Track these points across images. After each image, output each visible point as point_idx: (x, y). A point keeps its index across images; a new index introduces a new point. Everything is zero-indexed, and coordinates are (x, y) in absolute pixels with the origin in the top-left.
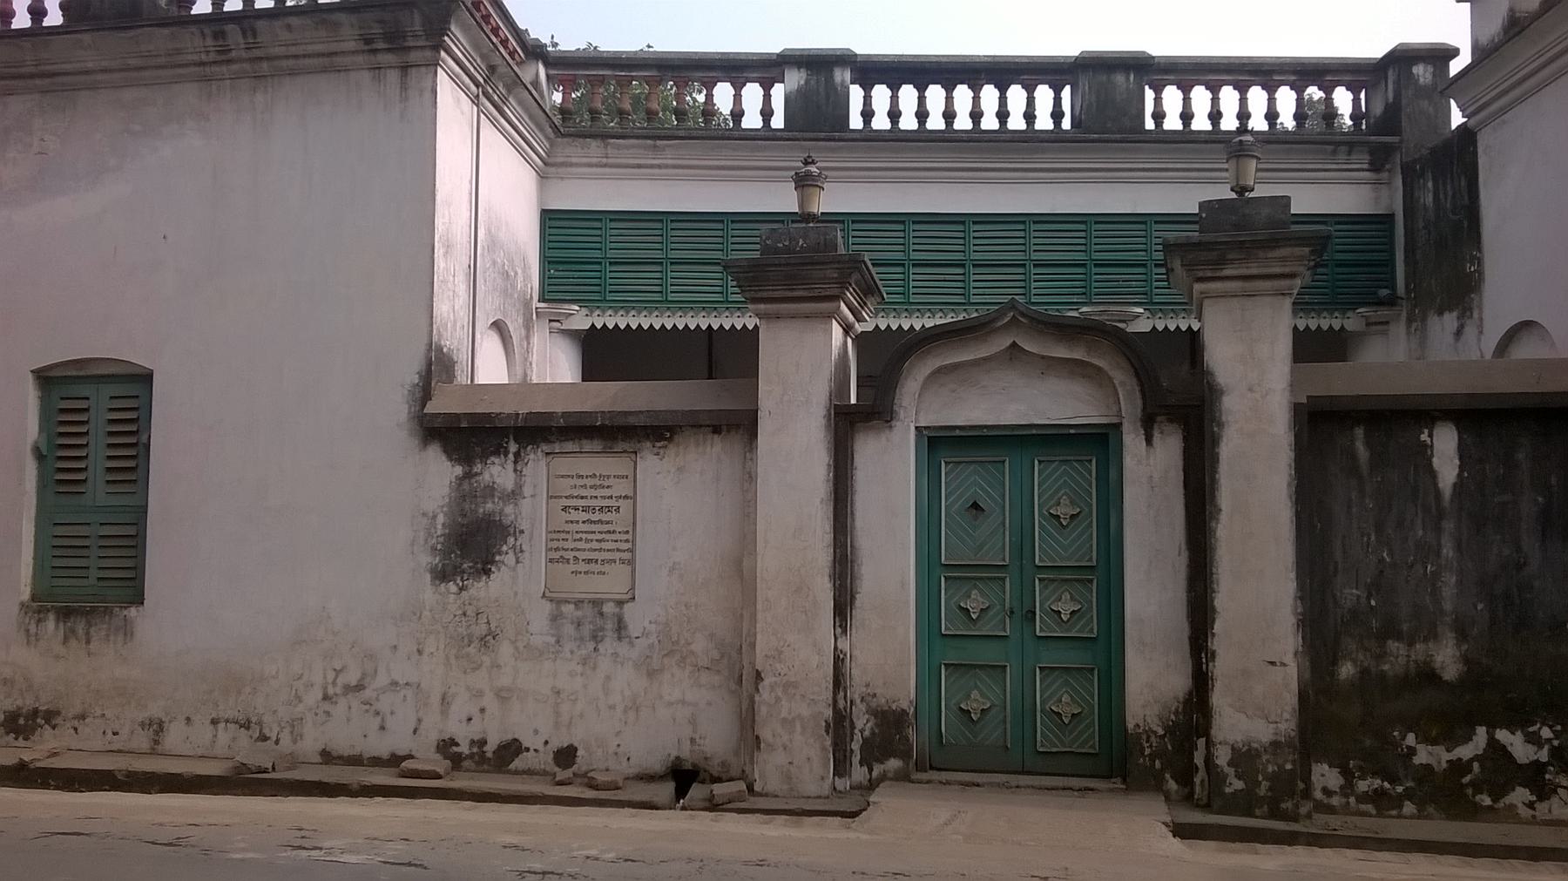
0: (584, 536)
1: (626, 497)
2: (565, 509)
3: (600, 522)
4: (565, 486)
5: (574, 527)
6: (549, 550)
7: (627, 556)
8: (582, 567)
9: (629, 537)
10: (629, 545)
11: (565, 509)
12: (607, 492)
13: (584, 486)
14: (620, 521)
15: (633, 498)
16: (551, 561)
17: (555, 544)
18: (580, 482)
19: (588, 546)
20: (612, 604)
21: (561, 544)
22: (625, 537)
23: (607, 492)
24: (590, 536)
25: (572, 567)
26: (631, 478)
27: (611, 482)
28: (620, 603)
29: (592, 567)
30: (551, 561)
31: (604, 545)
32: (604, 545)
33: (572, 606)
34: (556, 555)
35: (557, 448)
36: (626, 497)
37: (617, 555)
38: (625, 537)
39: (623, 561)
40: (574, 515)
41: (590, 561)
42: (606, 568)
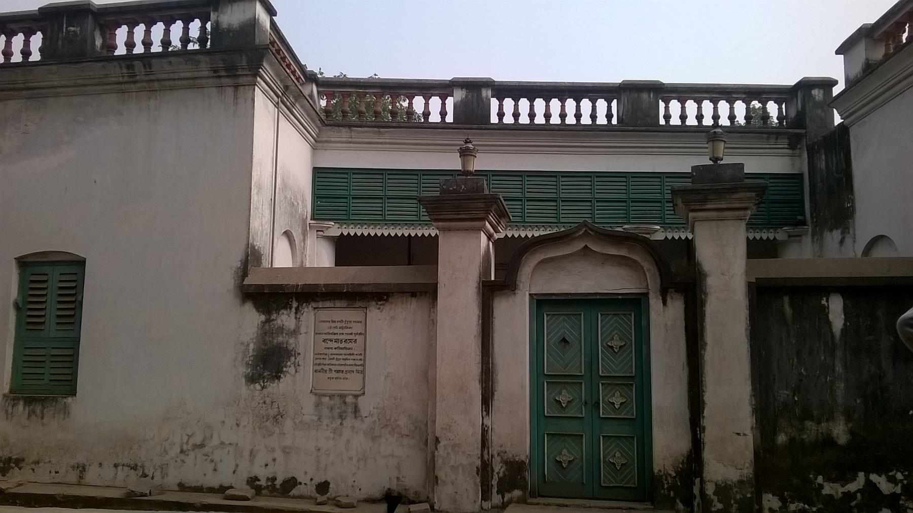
0: (335, 357)
1: (360, 334)
2: (324, 341)
3: (345, 348)
4: (325, 327)
5: (330, 351)
6: (314, 365)
7: (360, 368)
8: (334, 375)
9: (362, 357)
10: (362, 362)
11: (324, 341)
12: (349, 331)
13: (336, 327)
14: (357, 348)
15: (364, 334)
16: (316, 371)
17: (318, 361)
18: (334, 325)
19: (337, 363)
20: (351, 397)
21: (322, 361)
22: (359, 357)
23: (349, 331)
24: (339, 357)
25: (328, 375)
26: (363, 323)
27: (352, 324)
28: (356, 396)
29: (340, 375)
30: (316, 371)
31: (348, 362)
32: (348, 362)
33: (328, 398)
34: (319, 368)
35: (320, 305)
36: (360, 334)
37: (355, 368)
38: (359, 357)
39: (358, 372)
40: (330, 344)
41: (338, 371)
42: (348, 375)
